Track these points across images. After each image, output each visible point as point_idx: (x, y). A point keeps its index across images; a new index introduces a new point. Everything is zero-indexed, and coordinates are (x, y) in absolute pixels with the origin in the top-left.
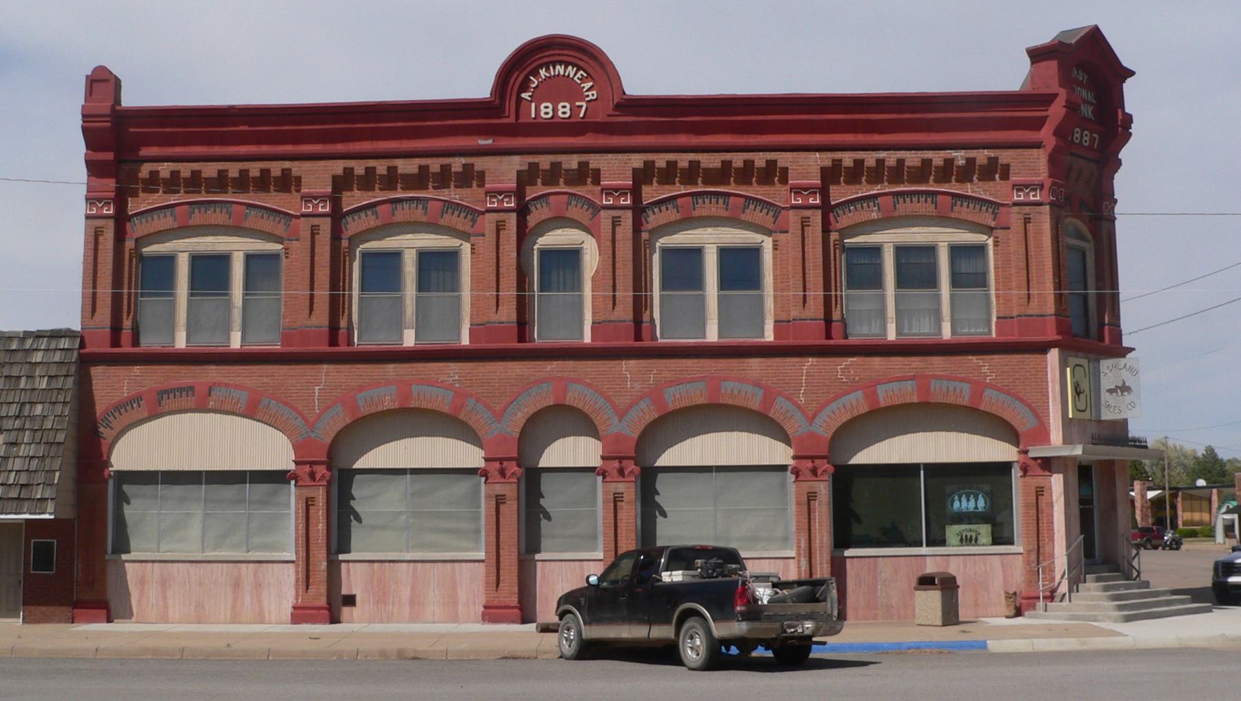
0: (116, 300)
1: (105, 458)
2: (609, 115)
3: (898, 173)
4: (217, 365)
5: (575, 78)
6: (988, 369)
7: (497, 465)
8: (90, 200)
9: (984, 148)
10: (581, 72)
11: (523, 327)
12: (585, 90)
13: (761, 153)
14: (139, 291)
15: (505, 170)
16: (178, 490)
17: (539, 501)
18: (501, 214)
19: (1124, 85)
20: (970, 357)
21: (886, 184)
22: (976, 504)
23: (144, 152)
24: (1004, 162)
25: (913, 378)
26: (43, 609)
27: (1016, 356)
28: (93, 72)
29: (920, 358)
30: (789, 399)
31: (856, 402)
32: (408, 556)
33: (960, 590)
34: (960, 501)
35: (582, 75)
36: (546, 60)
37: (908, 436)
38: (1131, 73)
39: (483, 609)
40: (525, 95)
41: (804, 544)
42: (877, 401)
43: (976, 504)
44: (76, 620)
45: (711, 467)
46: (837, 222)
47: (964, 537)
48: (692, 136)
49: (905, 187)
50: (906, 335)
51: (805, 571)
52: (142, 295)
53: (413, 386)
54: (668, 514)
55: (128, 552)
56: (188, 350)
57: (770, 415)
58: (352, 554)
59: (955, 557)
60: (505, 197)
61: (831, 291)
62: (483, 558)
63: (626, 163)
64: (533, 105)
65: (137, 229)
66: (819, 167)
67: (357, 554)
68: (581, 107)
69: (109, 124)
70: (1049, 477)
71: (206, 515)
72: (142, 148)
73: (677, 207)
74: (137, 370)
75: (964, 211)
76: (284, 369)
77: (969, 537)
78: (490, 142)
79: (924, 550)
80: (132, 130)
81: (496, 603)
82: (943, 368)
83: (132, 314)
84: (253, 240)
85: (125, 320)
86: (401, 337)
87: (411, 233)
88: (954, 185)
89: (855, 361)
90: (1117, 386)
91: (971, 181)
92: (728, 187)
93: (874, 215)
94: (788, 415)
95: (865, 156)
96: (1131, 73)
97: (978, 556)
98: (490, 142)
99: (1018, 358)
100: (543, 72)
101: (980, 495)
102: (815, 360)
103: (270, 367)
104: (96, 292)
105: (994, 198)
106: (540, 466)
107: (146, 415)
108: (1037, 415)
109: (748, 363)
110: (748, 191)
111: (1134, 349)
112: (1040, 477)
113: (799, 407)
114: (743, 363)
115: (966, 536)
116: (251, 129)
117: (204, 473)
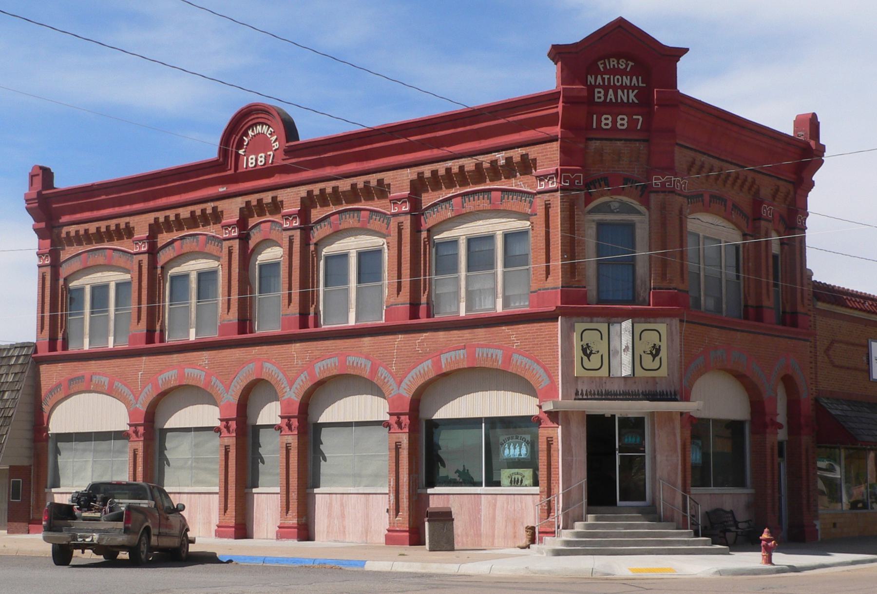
0: (53, 319)
1: (45, 425)
2: (283, 160)
3: (462, 177)
4: (96, 360)
5: (268, 134)
6: (515, 337)
7: (395, 418)
8: (40, 255)
9: (518, 147)
10: (271, 129)
11: (244, 323)
12: (272, 142)
13: (374, 175)
15: (232, 209)
16: (81, 445)
17: (258, 449)
18: (231, 241)
20: (504, 328)
21: (458, 187)
22: (520, 451)
23: (65, 219)
24: (532, 158)
25: (464, 347)
26: (16, 524)
27: (535, 325)
28: (32, 170)
29: (469, 331)
30: (386, 368)
31: (425, 370)
32: (186, 490)
33: (455, 522)
34: (509, 449)
35: (271, 131)
36: (250, 123)
37: (471, 395)
38: (679, 52)
39: (278, 529)
40: (241, 152)
41: (393, 483)
42: (441, 367)
43: (520, 451)
44: (30, 531)
45: (352, 422)
46: (426, 223)
47: (513, 480)
48: (333, 167)
49: (470, 188)
50: (477, 311)
51: (393, 504)
52: (71, 315)
53: (186, 369)
54: (327, 458)
56: (358, 326)
57: (208, 390)
59: (501, 496)
60: (233, 228)
62: (218, 491)
63: (298, 194)
64: (245, 158)
65: (429, 220)
66: (409, 180)
68: (270, 155)
70: (556, 429)
71: (94, 462)
72: (62, 217)
73: (489, 199)
74: (60, 366)
75: (512, 203)
76: (125, 361)
77: (516, 479)
78: (225, 189)
79: (483, 489)
80: (54, 206)
81: (223, 524)
82: (485, 338)
83: (427, 291)
84: (119, 273)
85: (422, 297)
86: (188, 335)
87: (193, 260)
88: (504, 182)
89: (428, 336)
91: (515, 176)
92: (360, 204)
93: (449, 215)
94: (386, 380)
95: (438, 167)
96: (679, 52)
97: (265, 495)
98: (225, 189)
99: (537, 326)
100: (250, 132)
102: (403, 336)
103: (119, 360)
104: (139, 305)
105: (530, 189)
106: (257, 424)
107: (63, 396)
108: (549, 376)
109: (363, 341)
110: (371, 205)
112: (550, 429)
113: (391, 373)
114: (360, 341)
115: (515, 479)
116: (107, 197)
117: (93, 434)
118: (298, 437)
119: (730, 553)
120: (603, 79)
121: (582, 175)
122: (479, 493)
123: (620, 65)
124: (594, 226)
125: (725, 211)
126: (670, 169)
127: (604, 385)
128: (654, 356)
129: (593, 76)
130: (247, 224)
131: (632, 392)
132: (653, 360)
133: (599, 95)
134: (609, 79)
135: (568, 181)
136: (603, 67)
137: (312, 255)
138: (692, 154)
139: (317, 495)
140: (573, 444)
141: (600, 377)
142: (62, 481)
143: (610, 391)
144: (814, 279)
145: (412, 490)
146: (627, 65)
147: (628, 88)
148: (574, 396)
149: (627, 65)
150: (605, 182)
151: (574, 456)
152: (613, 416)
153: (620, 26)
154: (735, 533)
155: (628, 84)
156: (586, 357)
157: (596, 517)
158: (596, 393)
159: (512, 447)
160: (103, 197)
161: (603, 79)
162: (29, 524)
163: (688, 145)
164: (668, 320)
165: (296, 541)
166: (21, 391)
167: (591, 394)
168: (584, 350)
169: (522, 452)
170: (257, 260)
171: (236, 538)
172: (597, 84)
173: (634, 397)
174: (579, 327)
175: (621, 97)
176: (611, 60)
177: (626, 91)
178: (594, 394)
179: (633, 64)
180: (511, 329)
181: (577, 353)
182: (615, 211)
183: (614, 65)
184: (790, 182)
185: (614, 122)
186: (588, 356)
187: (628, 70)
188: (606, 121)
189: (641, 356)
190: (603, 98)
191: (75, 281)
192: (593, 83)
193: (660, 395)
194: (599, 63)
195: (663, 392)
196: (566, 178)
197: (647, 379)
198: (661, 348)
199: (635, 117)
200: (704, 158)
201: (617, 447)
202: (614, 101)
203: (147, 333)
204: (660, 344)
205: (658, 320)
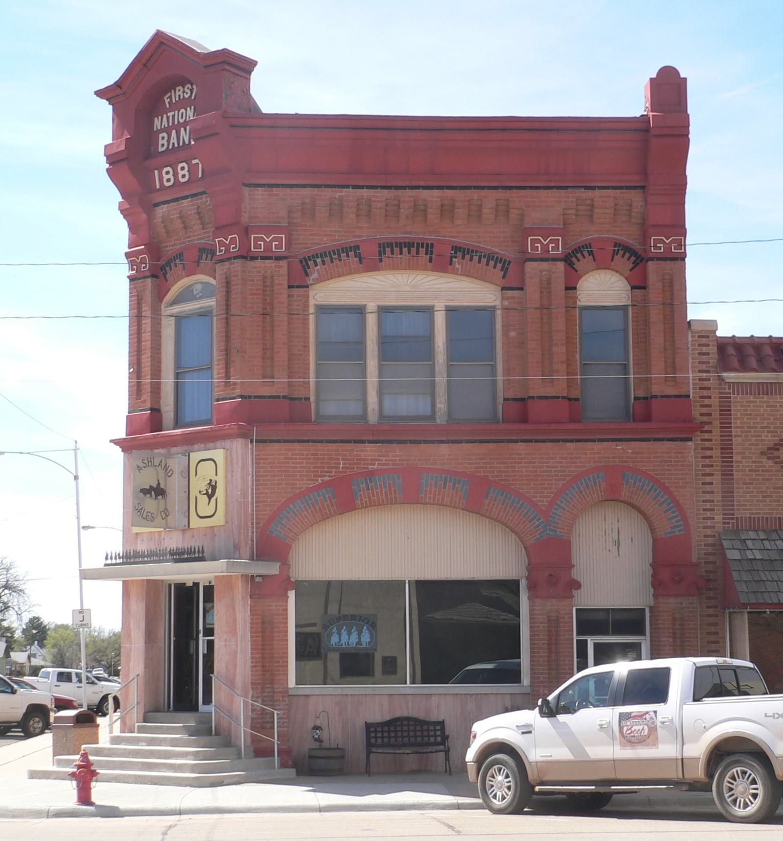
14: (691, 375)
22: (359, 638)
43: (359, 638)
61: (634, 377)
90: (151, 487)
101: (365, 628)
111: (111, 441)
121: (284, 236)
124: (172, 321)
127: (162, 543)
128: (210, 497)
134: (173, 116)
144: (719, 333)
152: (196, 585)
163: (299, 182)
164: (228, 443)
182: (198, 296)
189: (196, 498)
201: (201, 628)
204: (216, 478)
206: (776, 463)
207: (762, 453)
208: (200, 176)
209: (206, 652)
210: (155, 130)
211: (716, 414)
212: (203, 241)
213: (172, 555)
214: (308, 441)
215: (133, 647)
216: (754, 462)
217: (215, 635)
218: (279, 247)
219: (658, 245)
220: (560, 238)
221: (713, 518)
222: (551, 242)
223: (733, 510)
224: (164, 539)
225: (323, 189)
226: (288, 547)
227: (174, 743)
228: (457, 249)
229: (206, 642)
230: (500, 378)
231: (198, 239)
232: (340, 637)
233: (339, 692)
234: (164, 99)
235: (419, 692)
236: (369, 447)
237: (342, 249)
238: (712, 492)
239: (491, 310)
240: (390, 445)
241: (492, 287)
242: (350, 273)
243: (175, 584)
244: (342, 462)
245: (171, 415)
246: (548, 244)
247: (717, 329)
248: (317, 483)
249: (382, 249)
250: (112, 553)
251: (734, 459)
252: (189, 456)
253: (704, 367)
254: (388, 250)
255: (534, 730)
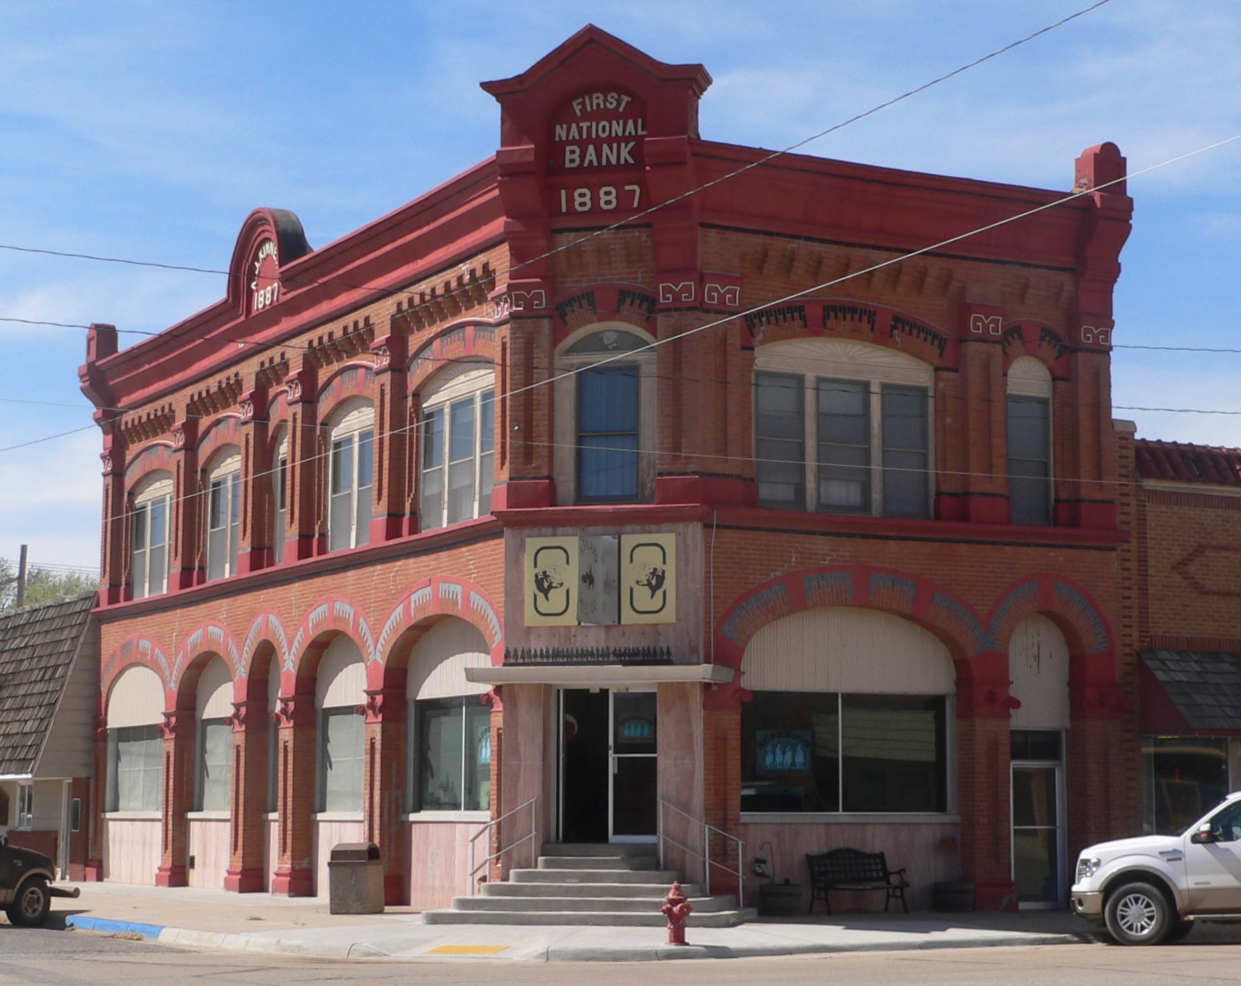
19: (499, 105)
22: (793, 759)
39: (226, 874)
43: (793, 759)
44: (87, 879)
55: (200, 809)
58: (120, 812)
66: (390, 316)
67: (210, 812)
69: (424, 405)
80: (111, 383)
101: (799, 746)
118: (294, 730)
119: (387, 909)
120: (580, 130)
122: (453, 820)
123: (607, 104)
125: (872, 329)
126: (688, 269)
127: (572, 640)
128: (654, 589)
129: (565, 126)
130: (265, 394)
131: (597, 650)
132: (652, 596)
133: (572, 156)
134: (589, 128)
135: (671, 296)
136: (580, 110)
137: (319, 441)
138: (760, 240)
139: (321, 824)
140: (521, 738)
141: (566, 626)
142: (122, 803)
143: (560, 649)
144: (1138, 436)
145: (389, 815)
146: (619, 102)
147: (619, 140)
148: (503, 660)
149: (619, 102)
150: (588, 301)
151: (522, 759)
152: (604, 693)
153: (591, 40)
154: (885, 892)
155: (620, 134)
156: (542, 594)
157: (546, 860)
158: (539, 653)
159: (778, 751)
160: (147, 367)
161: (580, 130)
162: (86, 866)
164: (680, 527)
165: (236, 894)
166: (72, 666)
167: (530, 656)
168: (539, 583)
169: (797, 760)
170: (279, 453)
171: (242, 891)
172: (571, 138)
173: (600, 659)
174: (532, 544)
175: (607, 157)
176: (595, 96)
177: (615, 145)
178: (535, 656)
179: (629, 99)
180: (471, 550)
181: (529, 587)
183: (598, 105)
184: (1064, 270)
185: (595, 199)
186: (546, 592)
187: (621, 110)
188: (582, 199)
189: (632, 590)
190: (578, 161)
191: (140, 496)
192: (564, 138)
193: (644, 654)
194: (574, 104)
195: (649, 649)
196: (518, 298)
197: (643, 629)
198: (666, 575)
199: (627, 188)
200: (793, 245)
201: (611, 742)
202: (595, 164)
203: (181, 573)
204: (664, 567)
205: (664, 526)
206: (1184, 578)
207: (1173, 568)
208: (635, 205)
209: (616, 772)
210: (557, 139)
211: (1134, 524)
212: (625, 282)
213: (615, 654)
214: (759, 529)
215: (522, 766)
216: (1166, 577)
217: (658, 752)
218: (733, 300)
219: (1086, 338)
220: (1001, 318)
221: (1131, 636)
222: (992, 321)
223: (1148, 627)
224: (575, 636)
225: (775, 237)
226: (741, 652)
227: (620, 878)
228: (897, 319)
229: (616, 760)
230: (932, 471)
231: (618, 280)
232: (774, 758)
233: (778, 820)
234: (572, 105)
235: (854, 821)
236: (820, 540)
237: (788, 309)
238: (1130, 607)
239: (923, 391)
240: (814, 536)
241: (925, 366)
242: (795, 335)
243: (564, 690)
244: (794, 556)
245: (571, 486)
246: (989, 324)
247: (1135, 431)
248: (770, 578)
249: (826, 313)
250: (516, 650)
251: (1149, 573)
252: (619, 537)
253: (1123, 471)
254: (832, 314)
255: (1184, 856)
